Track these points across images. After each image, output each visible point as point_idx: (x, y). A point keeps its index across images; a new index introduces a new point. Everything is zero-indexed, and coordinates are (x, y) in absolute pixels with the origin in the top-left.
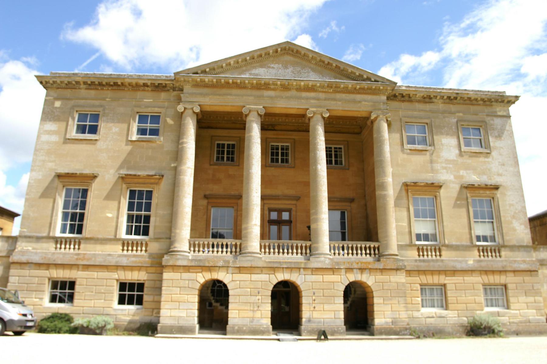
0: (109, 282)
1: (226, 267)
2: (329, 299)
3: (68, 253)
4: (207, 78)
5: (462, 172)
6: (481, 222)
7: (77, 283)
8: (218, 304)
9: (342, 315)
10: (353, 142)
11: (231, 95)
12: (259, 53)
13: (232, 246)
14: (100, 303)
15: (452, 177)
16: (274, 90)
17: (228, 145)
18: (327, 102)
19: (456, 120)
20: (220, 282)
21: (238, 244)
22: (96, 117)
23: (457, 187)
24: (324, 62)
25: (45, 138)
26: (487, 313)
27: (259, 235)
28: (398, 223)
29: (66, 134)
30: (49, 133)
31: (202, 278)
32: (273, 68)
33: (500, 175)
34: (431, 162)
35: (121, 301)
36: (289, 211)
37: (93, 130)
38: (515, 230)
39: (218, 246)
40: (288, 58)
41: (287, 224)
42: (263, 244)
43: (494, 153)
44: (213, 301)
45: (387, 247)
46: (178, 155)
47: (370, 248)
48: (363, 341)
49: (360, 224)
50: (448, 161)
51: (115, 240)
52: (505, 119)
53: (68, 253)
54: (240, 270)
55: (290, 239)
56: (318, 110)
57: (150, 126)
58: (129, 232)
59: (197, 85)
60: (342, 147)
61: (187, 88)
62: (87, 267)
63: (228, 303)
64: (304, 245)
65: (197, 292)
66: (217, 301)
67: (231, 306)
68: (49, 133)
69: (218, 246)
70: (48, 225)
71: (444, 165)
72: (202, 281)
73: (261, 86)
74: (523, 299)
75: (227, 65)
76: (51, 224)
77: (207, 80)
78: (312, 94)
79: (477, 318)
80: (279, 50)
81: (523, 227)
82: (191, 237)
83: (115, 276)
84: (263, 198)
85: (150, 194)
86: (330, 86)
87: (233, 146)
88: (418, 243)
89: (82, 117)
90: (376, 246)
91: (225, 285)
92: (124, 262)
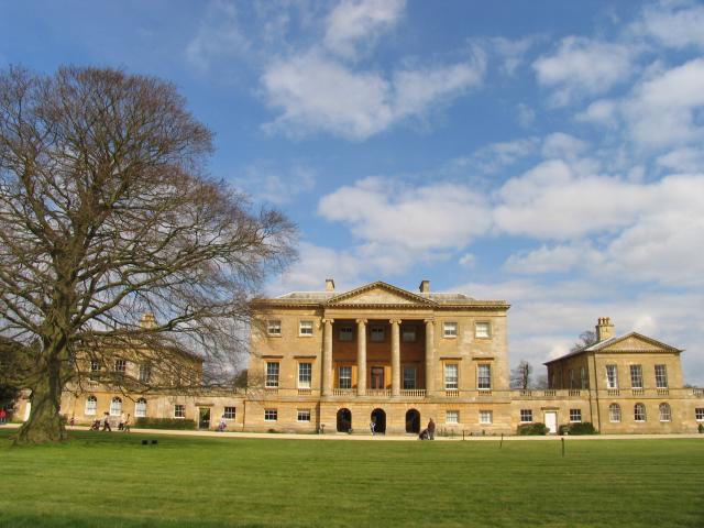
2: (398, 417)
5: (475, 351)
6: (453, 435)
9: (404, 425)
10: (416, 332)
14: (290, 420)
20: (346, 409)
28: (438, 374)
33: (495, 351)
34: (457, 345)
35: (267, 417)
43: (494, 339)
49: (415, 377)
50: (467, 344)
56: (396, 318)
79: (267, 294)
84: (368, 361)
85: (310, 365)
92: (300, 400)
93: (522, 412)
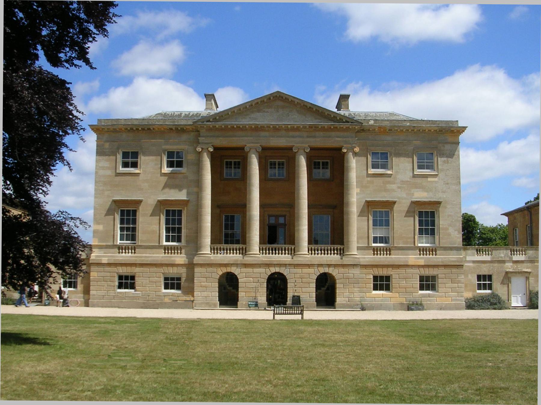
0: (158, 275)
1: (236, 265)
3: (126, 256)
4: (218, 125)
7: (137, 276)
8: (231, 288)
10: (330, 167)
11: (235, 136)
12: (256, 102)
13: (242, 249)
15: (404, 195)
16: (268, 131)
17: (235, 162)
18: (309, 139)
19: (412, 148)
21: (244, 247)
22: (135, 155)
23: (408, 203)
24: (306, 106)
25: (101, 172)
26: (421, 294)
27: (258, 241)
29: (116, 171)
30: (103, 168)
31: (221, 271)
32: (267, 112)
33: (444, 192)
36: (284, 216)
37: (135, 165)
38: (449, 235)
39: (224, 250)
40: (280, 103)
41: (277, 234)
42: (310, 248)
44: (227, 286)
45: (348, 248)
46: (198, 183)
47: (217, 249)
48: (329, 312)
49: (331, 232)
51: (160, 247)
52: (454, 145)
53: (126, 256)
54: (246, 265)
55: (285, 244)
57: (175, 161)
58: (167, 240)
59: (209, 129)
60: (329, 161)
61: (203, 132)
62: (142, 265)
63: (238, 287)
64: (339, 248)
65: (217, 281)
66: (230, 286)
67: (240, 290)
68: (103, 168)
69: (224, 250)
70: (112, 237)
71: (399, 185)
72: (221, 273)
73: (257, 129)
74: (449, 285)
75: (232, 112)
76: (114, 235)
77: (217, 126)
78: (297, 133)
80: (272, 98)
81: (456, 232)
82: (211, 244)
83: (161, 270)
85: (180, 212)
86: (311, 127)
87: (239, 162)
88: (374, 245)
89: (125, 155)
90: (342, 248)
91: (236, 276)
93: (479, 278)
